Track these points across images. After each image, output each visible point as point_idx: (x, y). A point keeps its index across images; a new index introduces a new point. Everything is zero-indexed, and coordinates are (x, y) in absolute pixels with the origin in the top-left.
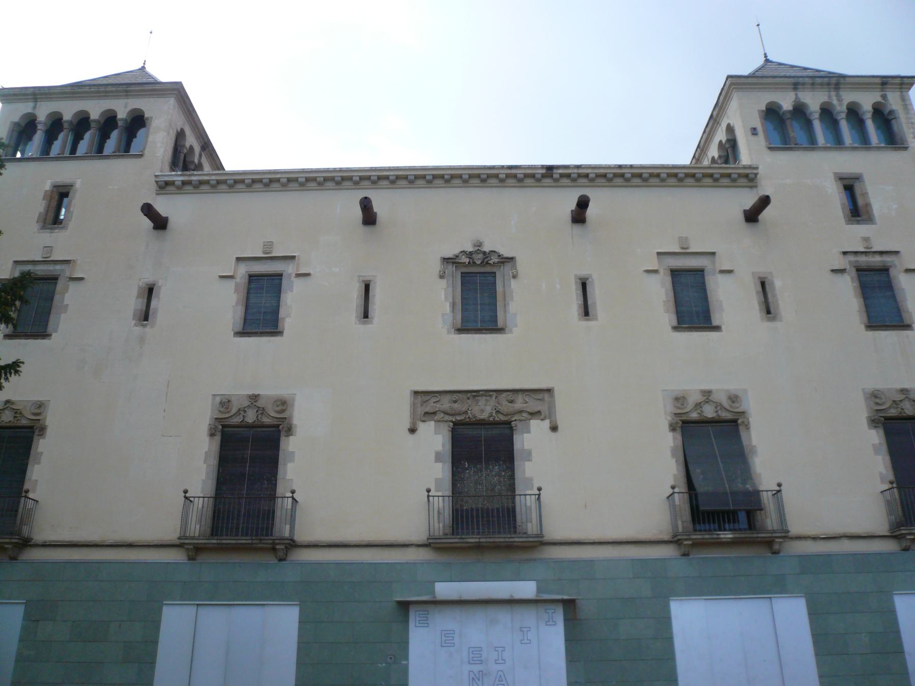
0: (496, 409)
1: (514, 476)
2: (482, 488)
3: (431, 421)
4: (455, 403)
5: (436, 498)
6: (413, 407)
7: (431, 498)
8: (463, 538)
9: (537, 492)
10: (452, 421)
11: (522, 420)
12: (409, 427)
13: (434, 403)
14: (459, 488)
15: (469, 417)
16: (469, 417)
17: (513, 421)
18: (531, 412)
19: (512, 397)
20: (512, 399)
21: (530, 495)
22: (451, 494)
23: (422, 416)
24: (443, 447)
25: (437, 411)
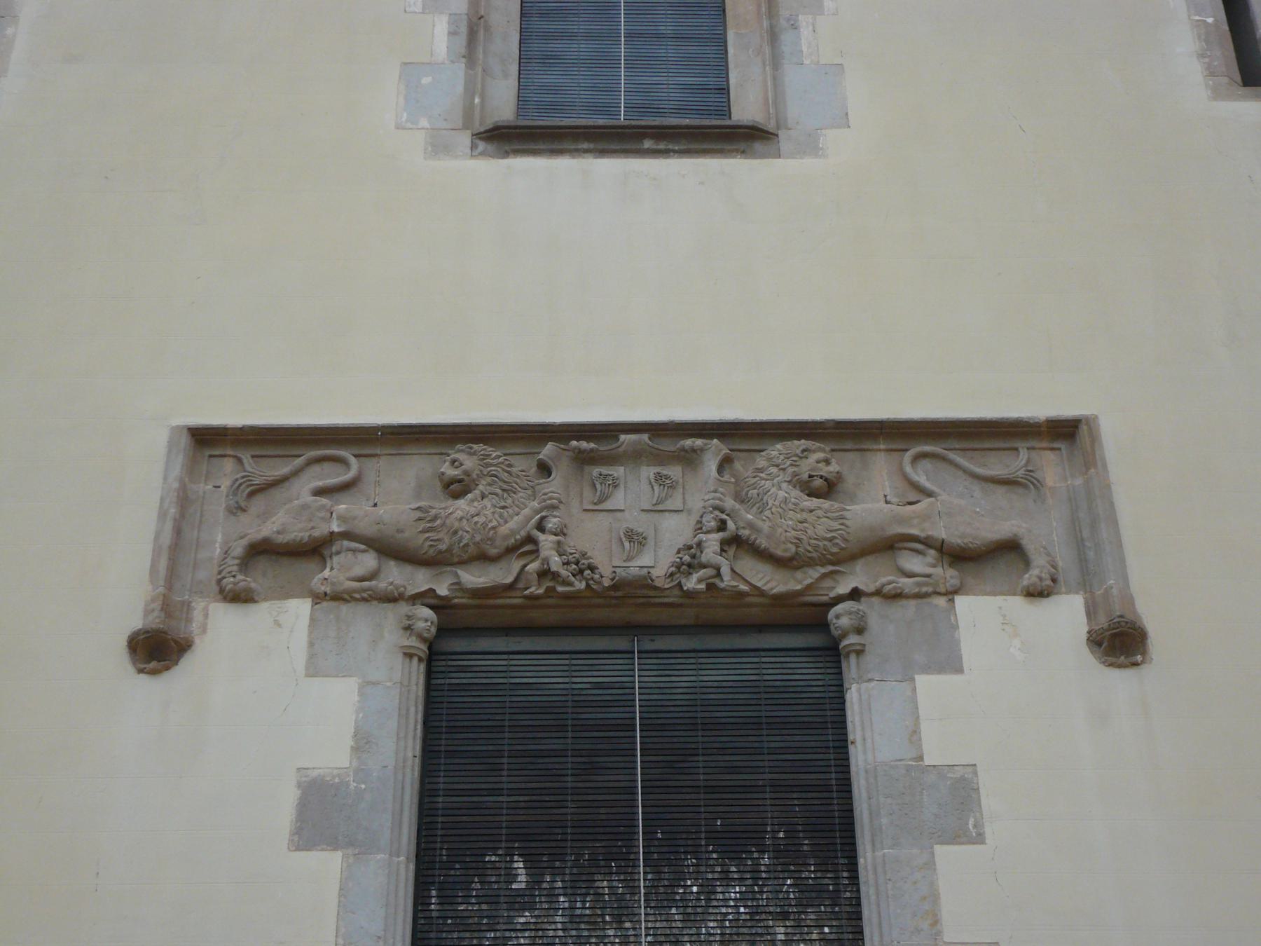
0: (722, 526)
4: (457, 496)
13: (320, 492)
16: (545, 573)
17: (840, 599)
19: (827, 462)
20: (834, 467)
24: (356, 749)
25: (332, 537)
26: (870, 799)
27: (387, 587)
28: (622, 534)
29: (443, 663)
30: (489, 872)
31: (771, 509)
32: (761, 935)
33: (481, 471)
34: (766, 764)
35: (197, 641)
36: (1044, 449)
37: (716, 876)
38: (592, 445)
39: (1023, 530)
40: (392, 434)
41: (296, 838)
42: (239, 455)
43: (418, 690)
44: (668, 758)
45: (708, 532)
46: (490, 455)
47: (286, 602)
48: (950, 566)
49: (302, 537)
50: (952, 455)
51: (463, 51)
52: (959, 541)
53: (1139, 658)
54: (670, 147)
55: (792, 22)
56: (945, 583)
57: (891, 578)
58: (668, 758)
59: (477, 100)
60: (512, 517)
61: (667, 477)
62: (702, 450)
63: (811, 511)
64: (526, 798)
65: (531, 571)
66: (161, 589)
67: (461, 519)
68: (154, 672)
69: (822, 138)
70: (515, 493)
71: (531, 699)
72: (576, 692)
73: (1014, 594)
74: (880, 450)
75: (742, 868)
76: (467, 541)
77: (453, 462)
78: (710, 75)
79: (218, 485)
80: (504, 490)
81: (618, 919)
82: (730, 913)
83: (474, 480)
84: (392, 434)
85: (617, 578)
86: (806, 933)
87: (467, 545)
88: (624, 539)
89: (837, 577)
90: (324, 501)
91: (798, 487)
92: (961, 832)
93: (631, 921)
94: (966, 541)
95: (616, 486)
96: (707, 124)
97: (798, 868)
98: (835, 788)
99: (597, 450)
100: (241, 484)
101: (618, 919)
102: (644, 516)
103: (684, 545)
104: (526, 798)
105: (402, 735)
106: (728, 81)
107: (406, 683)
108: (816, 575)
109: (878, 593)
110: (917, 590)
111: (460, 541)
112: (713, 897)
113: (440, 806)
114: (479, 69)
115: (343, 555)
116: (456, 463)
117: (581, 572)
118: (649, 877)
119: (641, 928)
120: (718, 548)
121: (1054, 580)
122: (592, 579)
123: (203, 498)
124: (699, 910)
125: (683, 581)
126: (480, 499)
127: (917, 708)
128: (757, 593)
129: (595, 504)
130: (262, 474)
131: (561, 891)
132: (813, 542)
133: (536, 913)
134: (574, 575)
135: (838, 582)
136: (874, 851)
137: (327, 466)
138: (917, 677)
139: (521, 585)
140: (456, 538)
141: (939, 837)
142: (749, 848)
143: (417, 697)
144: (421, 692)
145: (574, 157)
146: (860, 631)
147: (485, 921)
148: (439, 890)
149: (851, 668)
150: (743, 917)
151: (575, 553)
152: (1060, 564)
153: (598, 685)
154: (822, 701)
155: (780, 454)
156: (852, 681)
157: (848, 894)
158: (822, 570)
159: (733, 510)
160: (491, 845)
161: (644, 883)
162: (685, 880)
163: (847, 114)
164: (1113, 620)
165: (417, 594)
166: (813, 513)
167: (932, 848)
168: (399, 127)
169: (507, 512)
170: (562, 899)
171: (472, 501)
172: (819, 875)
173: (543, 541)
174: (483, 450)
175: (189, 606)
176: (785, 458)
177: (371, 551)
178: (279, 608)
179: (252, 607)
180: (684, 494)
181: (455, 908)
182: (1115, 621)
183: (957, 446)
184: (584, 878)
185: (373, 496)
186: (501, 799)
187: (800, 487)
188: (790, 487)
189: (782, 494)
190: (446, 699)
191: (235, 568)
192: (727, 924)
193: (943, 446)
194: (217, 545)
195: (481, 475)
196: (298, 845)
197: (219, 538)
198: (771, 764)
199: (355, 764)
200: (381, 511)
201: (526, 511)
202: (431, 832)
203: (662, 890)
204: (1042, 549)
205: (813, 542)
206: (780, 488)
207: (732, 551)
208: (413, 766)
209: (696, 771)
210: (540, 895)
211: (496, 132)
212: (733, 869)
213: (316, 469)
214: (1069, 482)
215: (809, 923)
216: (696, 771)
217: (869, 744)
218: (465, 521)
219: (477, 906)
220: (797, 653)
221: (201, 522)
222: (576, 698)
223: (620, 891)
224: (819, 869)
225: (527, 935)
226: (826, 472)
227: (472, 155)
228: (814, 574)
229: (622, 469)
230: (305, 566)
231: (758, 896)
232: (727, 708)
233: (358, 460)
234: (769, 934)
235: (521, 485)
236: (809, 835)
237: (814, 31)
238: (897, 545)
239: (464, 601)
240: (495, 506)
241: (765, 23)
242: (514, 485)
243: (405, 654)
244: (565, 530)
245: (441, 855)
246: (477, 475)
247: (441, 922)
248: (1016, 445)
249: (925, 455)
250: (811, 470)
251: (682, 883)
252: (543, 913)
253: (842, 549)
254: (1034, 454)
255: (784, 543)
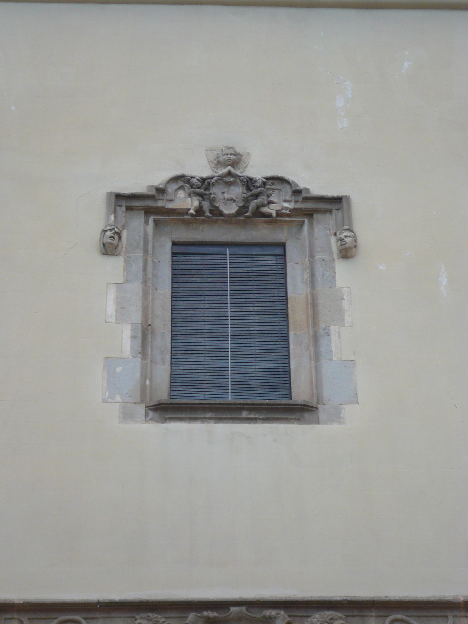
36: (462, 616)
38: (215, 614)
40: (105, 606)
42: (21, 619)
51: (140, 349)
54: (257, 416)
55: (327, 331)
59: (148, 382)
62: (275, 618)
69: (342, 411)
74: (372, 616)
78: (279, 362)
84: (105, 606)
96: (278, 403)
99: (218, 617)
106: (289, 366)
114: (149, 361)
145: (203, 423)
155: (318, 621)
163: (357, 394)
168: (104, 401)
174: (156, 617)
211: (159, 406)
227: (146, 421)
237: (339, 338)
241: (311, 331)
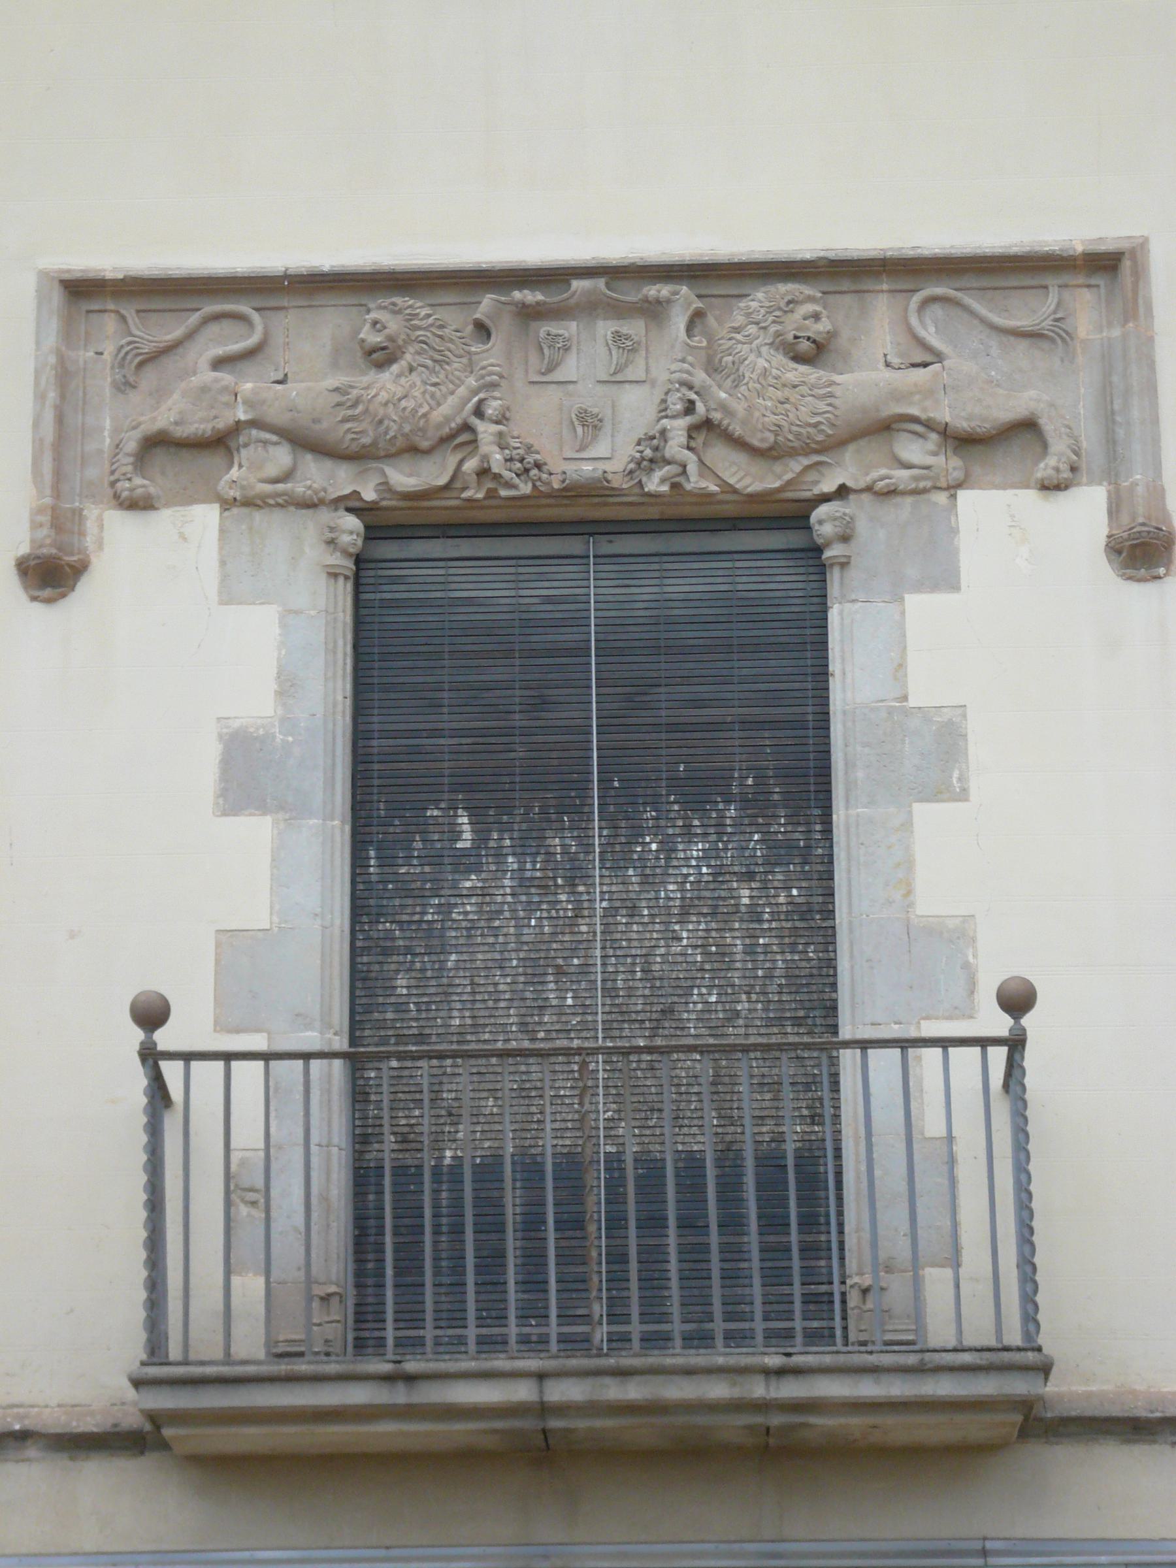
0: (690, 408)
1: (829, 913)
2: (584, 1009)
3: (190, 500)
4: (381, 366)
5: (208, 1074)
6: (52, 395)
7: (172, 1071)
8: (411, 1379)
9: (1000, 1024)
10: (353, 505)
11: (892, 493)
12: (25, 549)
13: (219, 363)
14: (401, 1008)
15: (484, 472)
16: (484, 472)
17: (826, 498)
18: (962, 424)
19: (816, 317)
20: (824, 326)
21: (945, 1043)
22: (340, 1043)
23: (126, 463)
24: (281, 694)
25: (238, 427)
26: (846, 746)
27: (305, 492)
28: (574, 416)
29: (372, 573)
30: (431, 828)
31: (747, 384)
32: (724, 899)
33: (408, 335)
34: (736, 695)
35: (94, 560)
37: (678, 831)
39: (1042, 405)
40: (300, 283)
41: (221, 801)
42: (123, 312)
43: (345, 617)
44: (628, 690)
45: (674, 417)
46: (417, 314)
47: (190, 508)
48: (955, 453)
49: (204, 431)
50: (968, 300)
52: (965, 425)
53: (1162, 571)
56: (946, 476)
57: (883, 471)
58: (628, 690)
60: (445, 397)
61: (628, 337)
63: (795, 387)
64: (469, 740)
65: (468, 472)
66: (48, 501)
67: (386, 404)
68: (49, 601)
70: (448, 364)
71: (473, 617)
72: (523, 608)
73: (1027, 487)
74: (882, 291)
75: (706, 821)
76: (393, 434)
77: (375, 323)
79: (100, 351)
80: (435, 361)
81: (571, 883)
82: (690, 875)
83: (400, 347)
84: (300, 283)
85: (567, 482)
86: (773, 896)
87: (395, 437)
88: (576, 423)
89: (823, 469)
90: (225, 377)
91: (781, 351)
92: (943, 787)
93: (585, 885)
94: (973, 424)
95: (567, 349)
97: (767, 820)
98: (811, 725)
99: (545, 303)
100: (127, 353)
101: (571, 883)
102: (601, 389)
103: (646, 434)
104: (469, 740)
105: (330, 674)
107: (331, 610)
108: (798, 468)
109: (869, 489)
110: (913, 486)
111: (386, 433)
112: (673, 856)
113: (375, 751)
115: (252, 447)
116: (378, 326)
117: (527, 471)
118: (605, 833)
119: (595, 892)
120: (683, 440)
121: (1073, 469)
122: (540, 479)
123: (85, 369)
124: (658, 871)
125: (644, 479)
126: (407, 374)
127: (905, 636)
128: (730, 489)
129: (543, 374)
130: (151, 338)
131: (509, 850)
132: (794, 428)
133: (483, 875)
134: (518, 475)
135: (823, 475)
136: (847, 808)
137: (227, 326)
138: (907, 596)
139: (458, 485)
140: (382, 429)
141: (920, 792)
142: (713, 798)
143: (345, 624)
144: (349, 619)
146: (845, 539)
147: (428, 886)
148: (378, 849)
149: (834, 578)
150: (706, 878)
151: (518, 448)
152: (1084, 445)
153: (549, 600)
154: (801, 616)
155: (761, 307)
156: (834, 601)
157: (820, 851)
158: (806, 461)
159: (703, 387)
160: (434, 796)
161: (600, 840)
162: (643, 836)
164: (1133, 528)
165: (339, 497)
166: (797, 389)
167: (910, 806)
169: (440, 390)
170: (510, 859)
171: (399, 376)
172: (789, 828)
173: (483, 433)
174: (410, 307)
175: (81, 515)
176: (767, 312)
177: (285, 443)
178: (183, 516)
179: (152, 515)
180: (647, 358)
181: (395, 871)
182: (1135, 530)
183: (975, 285)
184: (534, 834)
185: (282, 364)
186: (442, 741)
187: (784, 349)
188: (772, 351)
189: (761, 363)
190: (377, 619)
191: (130, 468)
192: (688, 886)
193: (958, 285)
194: (106, 433)
195: (409, 341)
196: (224, 810)
197: (108, 424)
198: (741, 695)
199: (280, 712)
200: (293, 390)
201: (462, 391)
202: (367, 782)
203: (618, 848)
204: (1063, 429)
205: (794, 428)
206: (759, 355)
207: (700, 438)
208: (344, 712)
209: (657, 705)
210: (487, 855)
212: (696, 823)
213: (214, 329)
214: (1105, 334)
215: (776, 884)
216: (657, 705)
217: (849, 680)
218: (391, 406)
219: (419, 868)
220: (778, 556)
221: (84, 403)
222: (524, 616)
223: (573, 849)
224: (791, 821)
225: (473, 901)
226: (815, 333)
228: (796, 466)
229: (573, 326)
230: (213, 460)
231: (722, 854)
232: (694, 627)
233: (260, 315)
234: (733, 898)
235: (457, 352)
236: (781, 780)
238: (894, 426)
239: (394, 503)
240: (426, 383)
242: (447, 353)
243: (329, 574)
244: (508, 414)
245: (379, 809)
246: (404, 340)
247: (381, 887)
248: (1044, 283)
249: (934, 299)
250: (797, 329)
251: (640, 840)
252: (490, 876)
253: (828, 436)
254: (1066, 294)
255: (761, 431)
